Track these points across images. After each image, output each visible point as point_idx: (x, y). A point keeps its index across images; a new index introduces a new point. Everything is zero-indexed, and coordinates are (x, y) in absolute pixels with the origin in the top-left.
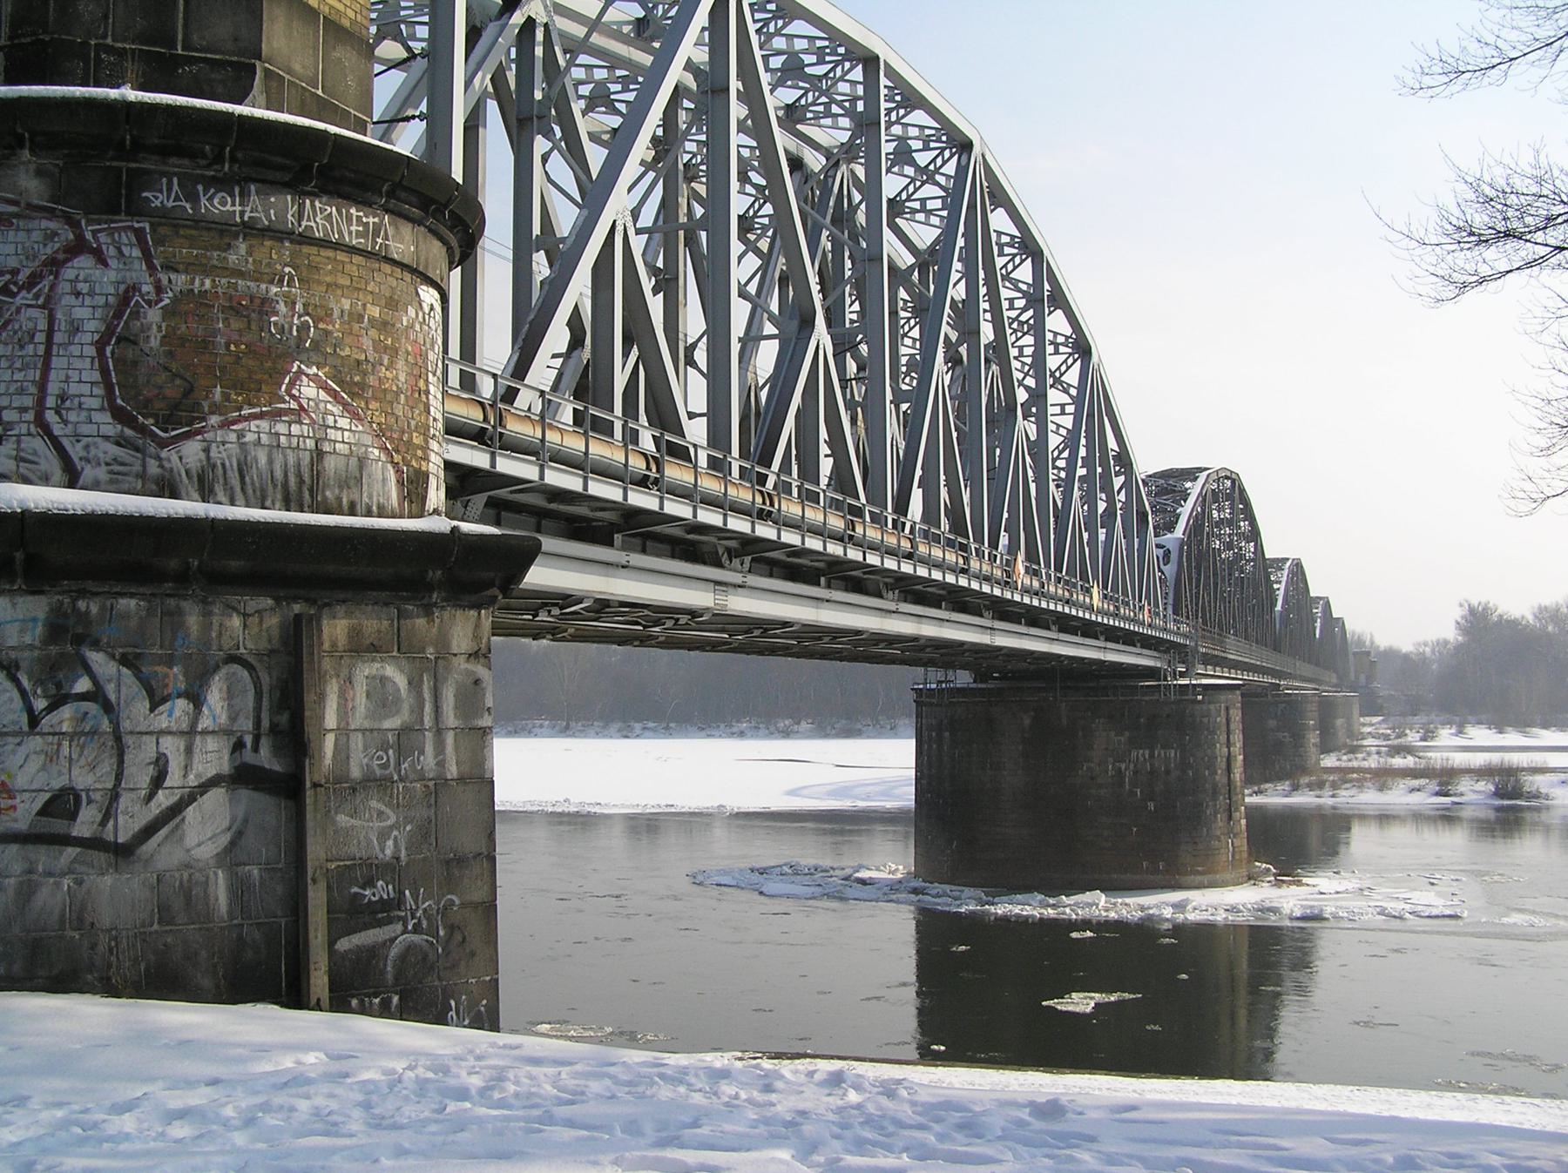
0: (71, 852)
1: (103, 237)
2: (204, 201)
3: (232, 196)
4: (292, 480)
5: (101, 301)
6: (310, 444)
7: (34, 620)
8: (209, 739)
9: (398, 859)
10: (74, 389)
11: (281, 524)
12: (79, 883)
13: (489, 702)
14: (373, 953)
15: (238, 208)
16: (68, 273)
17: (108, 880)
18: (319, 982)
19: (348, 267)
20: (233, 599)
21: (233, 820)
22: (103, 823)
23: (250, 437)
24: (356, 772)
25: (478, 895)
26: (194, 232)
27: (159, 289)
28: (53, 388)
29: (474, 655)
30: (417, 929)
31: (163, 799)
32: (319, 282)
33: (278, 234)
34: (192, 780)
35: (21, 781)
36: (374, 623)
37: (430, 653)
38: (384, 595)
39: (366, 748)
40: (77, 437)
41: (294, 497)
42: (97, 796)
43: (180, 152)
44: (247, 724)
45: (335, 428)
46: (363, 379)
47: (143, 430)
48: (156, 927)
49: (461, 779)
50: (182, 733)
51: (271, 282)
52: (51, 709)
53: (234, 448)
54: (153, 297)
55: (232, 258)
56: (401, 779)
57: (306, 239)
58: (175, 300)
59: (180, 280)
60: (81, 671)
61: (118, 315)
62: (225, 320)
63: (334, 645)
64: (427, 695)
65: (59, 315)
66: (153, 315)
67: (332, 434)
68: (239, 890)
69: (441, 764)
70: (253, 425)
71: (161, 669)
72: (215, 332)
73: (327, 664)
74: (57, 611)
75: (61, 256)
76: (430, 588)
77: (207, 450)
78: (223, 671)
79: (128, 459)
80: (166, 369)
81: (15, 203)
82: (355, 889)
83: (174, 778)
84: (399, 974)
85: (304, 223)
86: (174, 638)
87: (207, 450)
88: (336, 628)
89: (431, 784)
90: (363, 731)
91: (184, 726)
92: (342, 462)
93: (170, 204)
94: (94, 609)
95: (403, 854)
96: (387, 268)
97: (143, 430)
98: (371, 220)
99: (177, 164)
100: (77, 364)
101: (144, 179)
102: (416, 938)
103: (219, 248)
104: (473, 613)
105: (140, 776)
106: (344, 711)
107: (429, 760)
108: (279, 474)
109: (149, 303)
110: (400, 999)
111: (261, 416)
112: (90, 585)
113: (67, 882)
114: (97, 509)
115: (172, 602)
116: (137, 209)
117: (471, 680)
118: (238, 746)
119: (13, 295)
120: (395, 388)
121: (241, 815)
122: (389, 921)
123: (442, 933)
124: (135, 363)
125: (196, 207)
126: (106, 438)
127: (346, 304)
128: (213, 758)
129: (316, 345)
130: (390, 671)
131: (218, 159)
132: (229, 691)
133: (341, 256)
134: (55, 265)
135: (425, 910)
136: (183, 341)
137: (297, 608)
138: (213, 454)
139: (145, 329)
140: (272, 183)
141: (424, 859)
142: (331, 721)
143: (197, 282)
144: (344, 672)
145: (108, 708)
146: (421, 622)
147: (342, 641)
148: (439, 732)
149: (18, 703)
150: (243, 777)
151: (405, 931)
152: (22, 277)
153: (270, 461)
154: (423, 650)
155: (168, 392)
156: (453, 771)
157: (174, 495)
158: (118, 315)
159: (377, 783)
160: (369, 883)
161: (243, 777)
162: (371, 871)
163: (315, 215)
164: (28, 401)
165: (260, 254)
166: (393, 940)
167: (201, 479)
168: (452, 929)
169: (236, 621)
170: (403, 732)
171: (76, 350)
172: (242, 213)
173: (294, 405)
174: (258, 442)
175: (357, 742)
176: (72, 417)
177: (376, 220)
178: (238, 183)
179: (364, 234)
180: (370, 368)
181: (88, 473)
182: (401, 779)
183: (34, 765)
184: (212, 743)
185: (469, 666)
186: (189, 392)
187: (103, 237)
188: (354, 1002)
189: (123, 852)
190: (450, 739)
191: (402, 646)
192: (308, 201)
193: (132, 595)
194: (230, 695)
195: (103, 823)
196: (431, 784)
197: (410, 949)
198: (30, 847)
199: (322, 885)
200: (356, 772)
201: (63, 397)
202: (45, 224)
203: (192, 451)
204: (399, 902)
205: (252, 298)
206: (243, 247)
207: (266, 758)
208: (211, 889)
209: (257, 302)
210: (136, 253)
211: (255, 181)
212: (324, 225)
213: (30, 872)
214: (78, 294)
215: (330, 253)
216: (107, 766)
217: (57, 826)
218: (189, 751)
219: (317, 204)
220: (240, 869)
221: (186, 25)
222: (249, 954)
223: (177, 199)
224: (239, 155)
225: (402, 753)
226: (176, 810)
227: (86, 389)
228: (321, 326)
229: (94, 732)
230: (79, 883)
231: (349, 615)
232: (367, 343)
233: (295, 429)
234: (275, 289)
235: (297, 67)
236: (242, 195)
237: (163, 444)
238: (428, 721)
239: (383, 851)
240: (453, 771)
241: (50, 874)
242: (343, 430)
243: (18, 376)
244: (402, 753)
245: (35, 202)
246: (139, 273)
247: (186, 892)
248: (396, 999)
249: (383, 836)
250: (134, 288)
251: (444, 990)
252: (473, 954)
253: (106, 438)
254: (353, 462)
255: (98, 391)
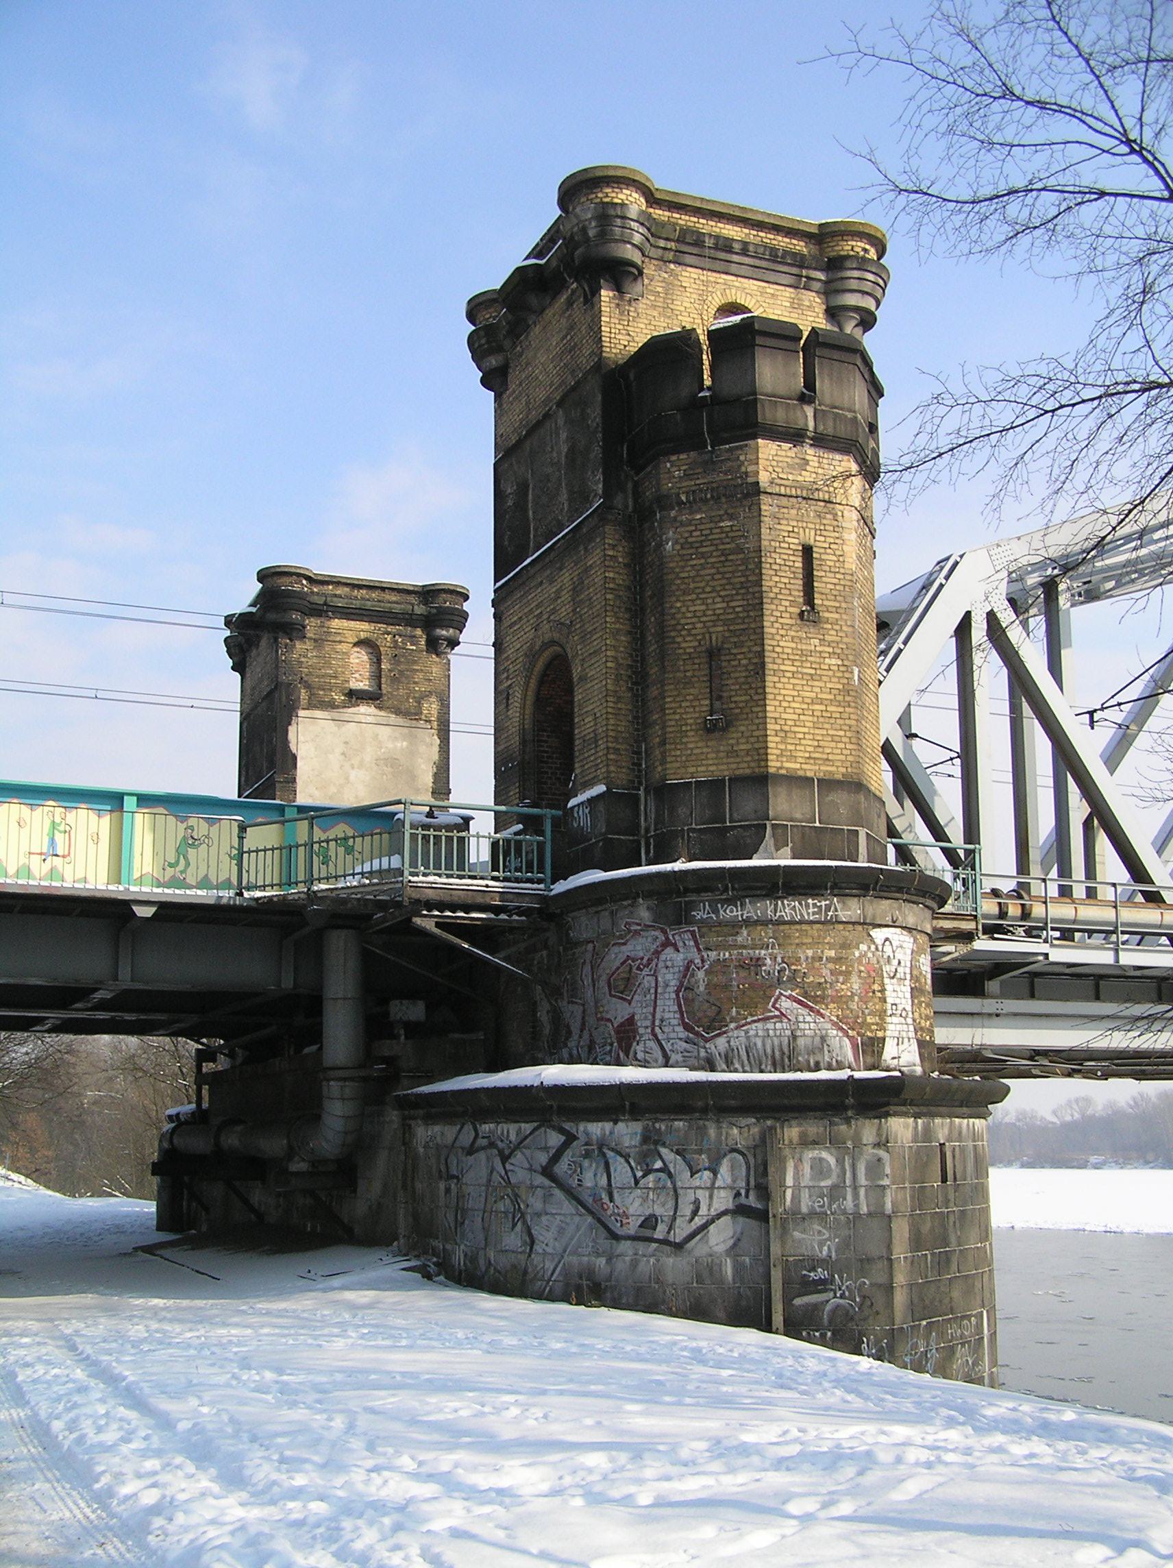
0: (654, 1245)
1: (677, 937)
2: (721, 912)
3: (736, 907)
4: (777, 1053)
5: (677, 969)
6: (788, 1033)
7: (636, 1133)
8: (722, 1191)
9: (830, 1257)
10: (667, 1016)
11: (740, 1082)
12: (658, 1261)
13: (888, 1170)
14: (816, 1307)
15: (740, 913)
16: (663, 957)
17: (671, 1260)
18: (778, 1319)
19: (810, 932)
20: (733, 1120)
21: (735, 1233)
22: (668, 1232)
23: (752, 1033)
24: (804, 1210)
25: (881, 1279)
26: (719, 929)
27: (703, 961)
28: (658, 1016)
29: (877, 1145)
30: (842, 1297)
31: (698, 1221)
32: (791, 944)
33: (765, 922)
34: (713, 1212)
35: (631, 1211)
36: (814, 1128)
37: (849, 1144)
38: (818, 1114)
39: (810, 1196)
40: (668, 1040)
41: (778, 1062)
42: (665, 1219)
43: (706, 889)
44: (742, 1184)
45: (805, 1022)
46: (824, 992)
47: (697, 1034)
48: (695, 1285)
49: (870, 1214)
50: (708, 1188)
51: (762, 948)
52: (644, 1176)
53: (743, 1040)
54: (700, 965)
55: (739, 939)
56: (832, 1214)
57: (781, 922)
58: (711, 965)
59: (713, 954)
60: (657, 1157)
61: (685, 976)
62: (737, 972)
63: (791, 1141)
64: (847, 1167)
65: (660, 979)
66: (701, 975)
67: (802, 1026)
68: (738, 1269)
69: (857, 1206)
70: (754, 1026)
71: (696, 1156)
72: (731, 980)
73: (787, 1152)
74: (646, 1129)
75: (660, 949)
76: (846, 1108)
77: (729, 1042)
78: (728, 1157)
79: (691, 1049)
80: (708, 1002)
81: (640, 925)
82: (804, 1272)
83: (703, 1210)
84: (830, 1322)
85: (778, 914)
86: (702, 1141)
87: (729, 1042)
88: (792, 1132)
89: (851, 1217)
90: (809, 1187)
91: (708, 1185)
92: (809, 1041)
93: (705, 916)
94: (663, 1128)
95: (833, 1255)
96: (841, 927)
97: (697, 1034)
98: (823, 903)
99: (706, 896)
100: (668, 1003)
101: (691, 906)
102: (841, 1301)
103: (732, 935)
104: (876, 1121)
105: (686, 1210)
106: (797, 1177)
107: (849, 1204)
108: (769, 1051)
109: (698, 968)
110: (833, 1334)
111: (759, 1020)
112: (659, 1116)
113: (652, 1260)
114: (624, 1080)
115: (701, 1122)
116: (690, 921)
117: (876, 1158)
118: (738, 1194)
119: (642, 970)
120: (849, 994)
121: (739, 1230)
122: (825, 1291)
123: (858, 1300)
124: (693, 1000)
125: (718, 917)
126: (681, 1039)
127: (810, 953)
128: (723, 1200)
129: (790, 979)
130: (824, 1155)
131: (726, 890)
132: (732, 1167)
133: (804, 927)
134: (657, 953)
135: (847, 1287)
136: (716, 986)
137: (769, 1123)
138: (732, 1043)
139: (697, 982)
140: (758, 896)
141: (846, 1259)
142: (789, 1181)
143: (722, 955)
144: (797, 1156)
145: (670, 1175)
146: (843, 1127)
147: (796, 1139)
148: (855, 1188)
149: (630, 1173)
150: (740, 1210)
151: (835, 1297)
152: (645, 961)
153: (764, 1045)
154: (845, 1143)
155: (709, 1014)
156: (864, 1209)
157: (713, 1070)
158: (685, 976)
159: (820, 1216)
160: (814, 1269)
161: (740, 1210)
162: (814, 1263)
163: (784, 908)
164: (648, 1023)
165: (755, 935)
166: (827, 1301)
167: (726, 1057)
168: (864, 1297)
169: (735, 1131)
170: (834, 1187)
171: (667, 996)
172: (742, 915)
173: (777, 1013)
174: (757, 1035)
175: (805, 1195)
176: (666, 1029)
177: (827, 902)
178: (739, 899)
179: (819, 912)
180: (828, 986)
181: (674, 1057)
182: (832, 1214)
183: (637, 1202)
184: (723, 1193)
185: (875, 1151)
186: (719, 1012)
187: (677, 937)
188: (804, 1333)
189: (679, 1247)
190: (862, 1192)
191: (835, 1142)
192: (779, 902)
193: (681, 1120)
194: (733, 1168)
195: (668, 1232)
196: (851, 1217)
197: (838, 1306)
198: (636, 1243)
199: (779, 1268)
200: (804, 1210)
201: (662, 1020)
202: (653, 933)
203: (721, 1042)
204: (832, 1281)
205: (751, 959)
206: (745, 933)
207: (753, 1201)
208: (723, 1269)
209: (754, 960)
210: (692, 943)
211: (747, 897)
212: (791, 914)
213: (636, 1254)
214: (667, 967)
215: (798, 927)
216: (671, 1204)
217: (647, 1233)
218: (711, 1197)
219: (786, 902)
220: (739, 1258)
221: (730, 809)
222: (744, 1303)
223: (709, 913)
224: (736, 886)
225: (832, 1199)
226: (704, 1227)
227: (671, 1015)
228: (793, 967)
229: (664, 1187)
230: (658, 1261)
231: (799, 1125)
232: (825, 972)
233: (778, 1025)
234: (763, 952)
235: (798, 816)
236: (741, 905)
237: (707, 1040)
238: (848, 1182)
239: (821, 1252)
240: (864, 1209)
241: (645, 1256)
242: (809, 1022)
243: (644, 1011)
244: (832, 1199)
245: (648, 923)
246: (694, 955)
247: (710, 1268)
248: (829, 1334)
249: (821, 1244)
250: (691, 962)
251: (860, 1333)
252: (877, 1313)
253: (681, 1039)
254: (817, 1039)
255: (677, 1016)
